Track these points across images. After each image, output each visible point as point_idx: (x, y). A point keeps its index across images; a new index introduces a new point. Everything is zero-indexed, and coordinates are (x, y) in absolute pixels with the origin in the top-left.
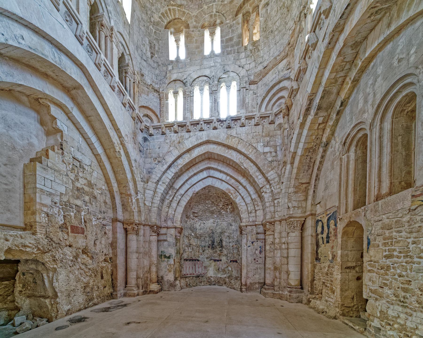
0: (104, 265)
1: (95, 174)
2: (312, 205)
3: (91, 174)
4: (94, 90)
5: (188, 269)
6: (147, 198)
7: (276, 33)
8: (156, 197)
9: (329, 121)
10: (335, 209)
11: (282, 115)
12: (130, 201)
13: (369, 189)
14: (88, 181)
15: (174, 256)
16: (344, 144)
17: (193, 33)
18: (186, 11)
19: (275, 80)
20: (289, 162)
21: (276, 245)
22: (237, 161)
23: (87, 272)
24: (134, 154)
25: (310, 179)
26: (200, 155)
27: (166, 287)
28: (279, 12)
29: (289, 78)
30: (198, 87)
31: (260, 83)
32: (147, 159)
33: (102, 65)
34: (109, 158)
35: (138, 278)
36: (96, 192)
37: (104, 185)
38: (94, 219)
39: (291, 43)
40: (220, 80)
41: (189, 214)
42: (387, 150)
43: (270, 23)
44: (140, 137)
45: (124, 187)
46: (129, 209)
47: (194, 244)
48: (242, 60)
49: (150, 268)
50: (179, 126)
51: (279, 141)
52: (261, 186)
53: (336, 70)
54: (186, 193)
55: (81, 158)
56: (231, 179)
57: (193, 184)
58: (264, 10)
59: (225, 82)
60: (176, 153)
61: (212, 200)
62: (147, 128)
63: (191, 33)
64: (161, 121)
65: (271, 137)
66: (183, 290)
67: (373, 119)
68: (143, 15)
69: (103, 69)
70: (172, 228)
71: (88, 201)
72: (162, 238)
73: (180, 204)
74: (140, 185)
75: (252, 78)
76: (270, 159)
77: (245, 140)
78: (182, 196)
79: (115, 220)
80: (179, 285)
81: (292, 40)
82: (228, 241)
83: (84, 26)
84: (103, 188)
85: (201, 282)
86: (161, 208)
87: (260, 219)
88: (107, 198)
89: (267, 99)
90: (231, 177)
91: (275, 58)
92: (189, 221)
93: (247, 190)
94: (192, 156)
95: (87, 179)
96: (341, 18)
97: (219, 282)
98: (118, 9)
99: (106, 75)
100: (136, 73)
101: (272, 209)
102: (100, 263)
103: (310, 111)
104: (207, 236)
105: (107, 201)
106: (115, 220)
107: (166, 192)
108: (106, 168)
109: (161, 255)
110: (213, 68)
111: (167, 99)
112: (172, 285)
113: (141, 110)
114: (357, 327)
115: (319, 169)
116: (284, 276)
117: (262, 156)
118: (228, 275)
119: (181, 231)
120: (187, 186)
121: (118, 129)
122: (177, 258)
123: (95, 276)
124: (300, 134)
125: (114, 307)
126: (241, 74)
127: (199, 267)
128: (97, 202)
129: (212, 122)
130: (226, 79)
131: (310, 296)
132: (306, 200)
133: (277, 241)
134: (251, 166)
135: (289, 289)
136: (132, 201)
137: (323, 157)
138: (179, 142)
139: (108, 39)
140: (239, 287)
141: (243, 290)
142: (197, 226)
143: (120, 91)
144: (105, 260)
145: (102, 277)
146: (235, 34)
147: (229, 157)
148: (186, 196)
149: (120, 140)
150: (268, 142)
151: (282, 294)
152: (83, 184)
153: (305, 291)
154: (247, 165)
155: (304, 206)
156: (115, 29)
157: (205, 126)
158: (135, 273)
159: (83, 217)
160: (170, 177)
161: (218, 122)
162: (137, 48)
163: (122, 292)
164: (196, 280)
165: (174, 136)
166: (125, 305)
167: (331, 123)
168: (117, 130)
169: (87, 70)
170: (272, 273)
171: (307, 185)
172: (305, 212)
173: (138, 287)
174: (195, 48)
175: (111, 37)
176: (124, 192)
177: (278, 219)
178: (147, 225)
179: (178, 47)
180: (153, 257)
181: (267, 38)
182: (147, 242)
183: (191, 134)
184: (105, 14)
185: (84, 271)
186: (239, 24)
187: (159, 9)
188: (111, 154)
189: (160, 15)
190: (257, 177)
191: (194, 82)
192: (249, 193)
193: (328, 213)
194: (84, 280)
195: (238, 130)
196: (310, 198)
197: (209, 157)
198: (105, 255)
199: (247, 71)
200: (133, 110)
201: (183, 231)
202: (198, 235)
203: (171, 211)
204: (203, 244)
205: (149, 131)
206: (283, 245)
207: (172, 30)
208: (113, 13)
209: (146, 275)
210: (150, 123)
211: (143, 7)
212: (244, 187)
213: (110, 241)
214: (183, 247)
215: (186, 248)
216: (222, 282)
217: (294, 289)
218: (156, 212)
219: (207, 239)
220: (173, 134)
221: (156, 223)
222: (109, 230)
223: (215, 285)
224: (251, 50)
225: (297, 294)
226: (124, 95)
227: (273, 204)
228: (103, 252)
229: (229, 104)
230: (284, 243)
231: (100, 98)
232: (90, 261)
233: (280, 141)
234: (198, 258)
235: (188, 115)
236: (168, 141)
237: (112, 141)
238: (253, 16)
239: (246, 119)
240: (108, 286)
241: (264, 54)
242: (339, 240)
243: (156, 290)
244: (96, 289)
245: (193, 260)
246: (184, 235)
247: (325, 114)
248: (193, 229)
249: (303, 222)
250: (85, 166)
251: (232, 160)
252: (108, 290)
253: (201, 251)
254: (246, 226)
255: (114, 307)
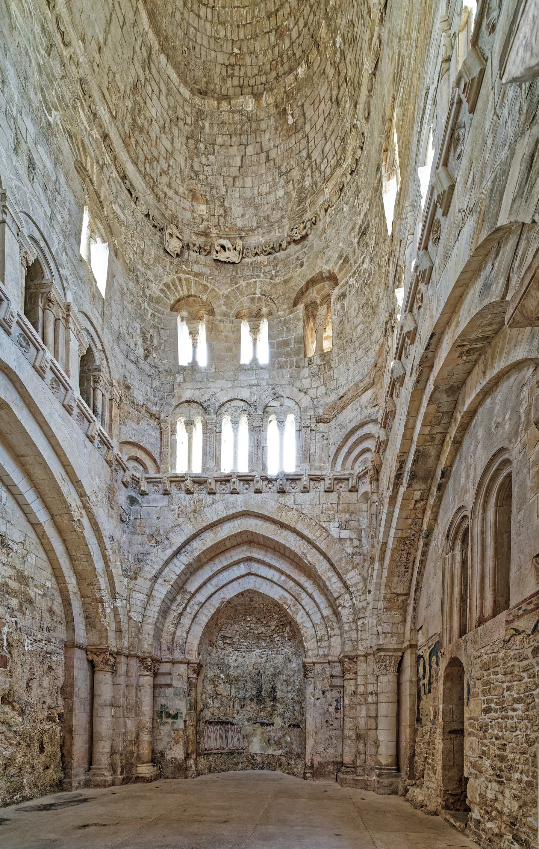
0: (47, 727)
1: (32, 559)
2: (412, 630)
3: (24, 558)
4: (31, 412)
5: (212, 738)
6: (135, 606)
7: (357, 344)
8: (152, 607)
9: (430, 497)
10: (437, 638)
11: (367, 479)
12: (100, 610)
13: (470, 609)
14: (18, 571)
15: (184, 714)
16: (448, 536)
17: (221, 324)
18: (208, 284)
19: (355, 420)
20: (377, 558)
21: (359, 697)
22: (297, 551)
23: (11, 738)
24: (109, 526)
25: (409, 588)
26: (232, 536)
27: (169, 770)
28: (361, 311)
29: (375, 421)
30: (229, 418)
31: (333, 423)
32: (136, 537)
33: (48, 370)
34: (60, 531)
35: (113, 753)
36: (33, 592)
37: (50, 580)
38: (27, 641)
39: (378, 365)
40: (268, 409)
41: (215, 639)
42: (490, 552)
43: (347, 327)
44: (122, 497)
45: (88, 585)
46: (98, 625)
47: (225, 694)
48: (304, 381)
49: (137, 736)
50: (194, 482)
51: (364, 522)
52: (335, 595)
53: (430, 422)
54: (209, 601)
55: (4, 529)
56: (288, 580)
57: (221, 585)
58: (339, 304)
59: (275, 413)
60: (189, 529)
61: (259, 617)
62: (136, 481)
63: (218, 323)
64: (162, 470)
65: (352, 513)
66: (202, 777)
67: (475, 505)
68: (131, 284)
69: (49, 375)
70: (181, 663)
71: (17, 608)
72: (162, 680)
73: (197, 620)
74: (121, 583)
75: (321, 412)
76: (350, 551)
77: (309, 515)
78: (202, 605)
79: (70, 645)
80: (194, 768)
81: (380, 360)
82: (285, 690)
83: (13, 304)
84: (48, 584)
85: (237, 764)
86: (160, 626)
87: (336, 652)
88: (56, 603)
89: (345, 450)
90: (288, 576)
91: (356, 385)
92: (215, 651)
93: (315, 601)
94: (218, 536)
95: (14, 567)
96: (426, 349)
97: (269, 763)
98: (82, 273)
99: (55, 386)
100: (115, 383)
101: (354, 635)
102: (39, 723)
103: (402, 479)
104: (248, 679)
105: (55, 608)
106: (70, 645)
107: (171, 598)
108: (53, 550)
109: (161, 712)
110: (255, 388)
111: (174, 432)
112: (181, 769)
113: (124, 449)
114: (457, 824)
115: (420, 573)
116: (371, 750)
117: (337, 545)
118: (285, 751)
119: (199, 668)
120: (210, 589)
121: (78, 481)
122: (190, 718)
123: (28, 746)
124: (390, 514)
125: (63, 804)
126: (303, 404)
127: (233, 737)
128: (35, 610)
129: (252, 480)
130: (278, 410)
131: (408, 781)
132: (404, 622)
133: (361, 689)
134: (319, 561)
135: (377, 771)
136: (104, 610)
137: (424, 554)
138: (195, 511)
139: (61, 325)
140: (302, 772)
141: (308, 775)
142: (231, 661)
143: (83, 415)
144: (49, 719)
145: (42, 750)
146: (293, 337)
147: (283, 542)
148: (209, 607)
149: (82, 501)
150: (347, 522)
151: (367, 780)
152: (7, 575)
153: (403, 773)
154: (312, 557)
155: (401, 631)
156: (75, 308)
157: (240, 487)
158: (108, 744)
159: (5, 637)
160: (178, 572)
161: (263, 480)
162: (119, 339)
163: (82, 777)
164: (228, 759)
165: (186, 500)
166: (85, 800)
167: (431, 502)
168: (76, 483)
169: (17, 376)
170: (353, 745)
171: (406, 597)
172: (403, 642)
173: (114, 771)
174: (224, 351)
175: (67, 321)
176: (90, 594)
177: (363, 653)
178: (133, 656)
179: (195, 345)
180: (144, 715)
181: (344, 350)
182: (132, 686)
183: (217, 497)
184: (56, 283)
185: (6, 736)
186: (298, 320)
187: (161, 276)
188: (64, 522)
189: (161, 286)
190: (329, 579)
191: (222, 408)
192: (318, 606)
193: (430, 644)
194: (5, 752)
195: (297, 498)
196: (409, 618)
197: (249, 539)
198: (49, 708)
199: (312, 399)
200: (109, 448)
201: (204, 669)
202: (232, 678)
203: (180, 633)
204: (241, 694)
205: (140, 487)
206: (370, 697)
207: (184, 313)
208: (71, 279)
209: (130, 748)
210: (140, 476)
211: (131, 271)
212: (310, 596)
213: (60, 682)
214: (204, 697)
215: (210, 701)
216: (274, 764)
217: (386, 771)
218: (151, 633)
219: (250, 685)
220: (183, 495)
221: (150, 653)
222: (58, 663)
223: (262, 768)
224: (319, 366)
225: (390, 780)
226: (90, 422)
227: (354, 627)
228: (44, 702)
229: (283, 453)
230: (371, 694)
231: (43, 425)
232: (18, 719)
233: (366, 522)
234: (231, 720)
235: (211, 464)
236: (175, 507)
237: (65, 502)
238: (322, 310)
239: (311, 480)
240: (53, 767)
241: (340, 375)
242: (441, 687)
243: (148, 776)
244: (29, 771)
245: (222, 723)
246: (206, 677)
247: (423, 486)
248: (223, 667)
249: (399, 659)
250: (11, 543)
251: (288, 548)
252: (53, 774)
253: (237, 707)
254: (314, 663)
255: (63, 804)
